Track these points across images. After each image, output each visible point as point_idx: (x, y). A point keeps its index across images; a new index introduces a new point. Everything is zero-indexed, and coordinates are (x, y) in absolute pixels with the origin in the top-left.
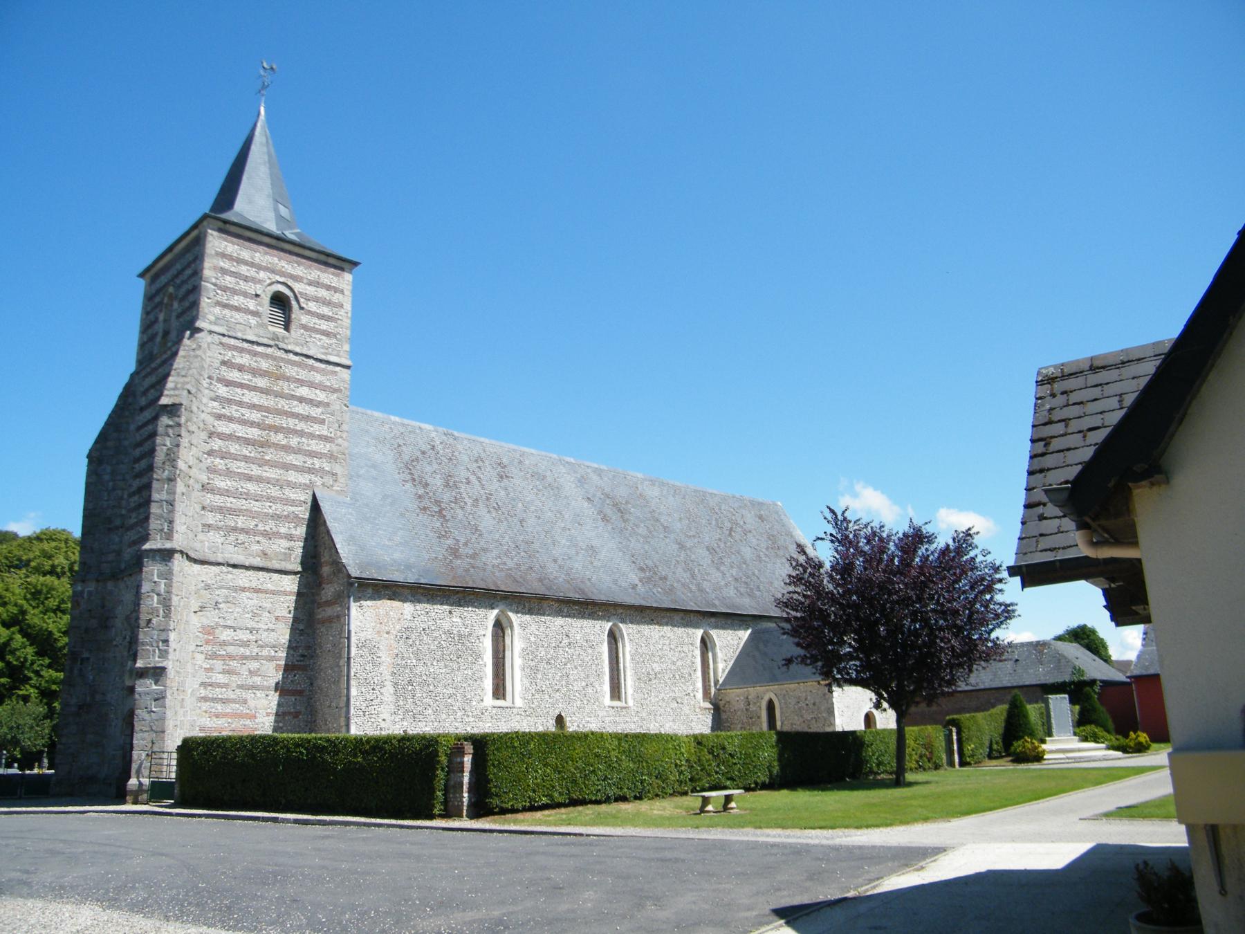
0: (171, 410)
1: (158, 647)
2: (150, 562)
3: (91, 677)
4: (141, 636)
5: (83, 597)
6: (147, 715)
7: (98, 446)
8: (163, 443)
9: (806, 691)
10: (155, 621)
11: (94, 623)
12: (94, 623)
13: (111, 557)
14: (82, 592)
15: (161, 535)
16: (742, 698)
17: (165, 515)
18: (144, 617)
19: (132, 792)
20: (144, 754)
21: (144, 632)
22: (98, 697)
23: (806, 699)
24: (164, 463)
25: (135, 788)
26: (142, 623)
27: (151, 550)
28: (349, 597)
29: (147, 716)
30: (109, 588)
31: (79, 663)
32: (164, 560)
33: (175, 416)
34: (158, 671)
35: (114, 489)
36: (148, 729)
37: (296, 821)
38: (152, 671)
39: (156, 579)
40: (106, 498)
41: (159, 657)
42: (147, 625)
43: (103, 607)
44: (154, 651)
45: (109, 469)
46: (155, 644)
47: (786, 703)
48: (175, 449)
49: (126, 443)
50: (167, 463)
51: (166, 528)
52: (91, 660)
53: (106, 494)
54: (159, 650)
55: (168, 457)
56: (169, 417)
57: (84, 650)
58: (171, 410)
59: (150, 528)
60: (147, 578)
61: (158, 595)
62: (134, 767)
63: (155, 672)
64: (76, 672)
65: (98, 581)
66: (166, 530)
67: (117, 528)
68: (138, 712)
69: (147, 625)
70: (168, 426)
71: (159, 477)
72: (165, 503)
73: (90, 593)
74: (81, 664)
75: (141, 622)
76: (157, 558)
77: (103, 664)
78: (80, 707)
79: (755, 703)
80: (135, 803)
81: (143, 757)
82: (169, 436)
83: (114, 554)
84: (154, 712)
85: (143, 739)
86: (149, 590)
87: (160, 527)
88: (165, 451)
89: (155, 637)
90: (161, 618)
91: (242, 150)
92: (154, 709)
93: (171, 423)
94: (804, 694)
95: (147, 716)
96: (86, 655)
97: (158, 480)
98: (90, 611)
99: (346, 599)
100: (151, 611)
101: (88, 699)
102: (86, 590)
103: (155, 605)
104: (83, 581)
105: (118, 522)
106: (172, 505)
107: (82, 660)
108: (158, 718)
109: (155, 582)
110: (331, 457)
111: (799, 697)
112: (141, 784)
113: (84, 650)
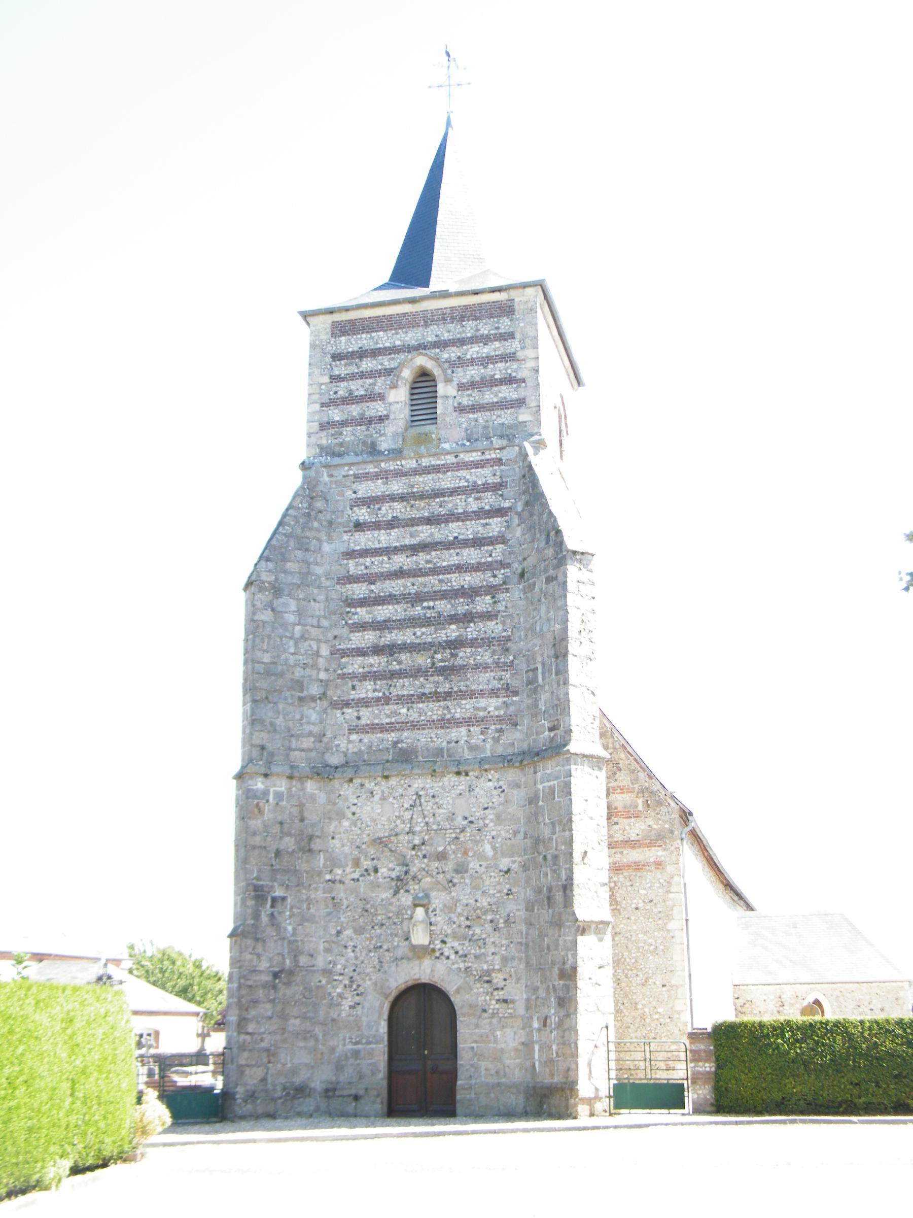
3: (290, 928)
11: (289, 843)
12: (289, 843)
13: (307, 743)
16: (772, 997)
22: (303, 960)
23: (655, 1029)
30: (309, 790)
31: (269, 903)
35: (303, 638)
37: (711, 1123)
40: (292, 650)
45: (293, 605)
47: (840, 1007)
52: (289, 900)
53: (291, 643)
57: (275, 884)
64: (264, 919)
73: (279, 796)
74: (272, 906)
77: (309, 909)
78: (276, 975)
79: (792, 1005)
83: (312, 739)
91: (441, 145)
94: (868, 997)
96: (279, 892)
98: (281, 823)
101: (288, 961)
107: (274, 900)
110: (351, 603)
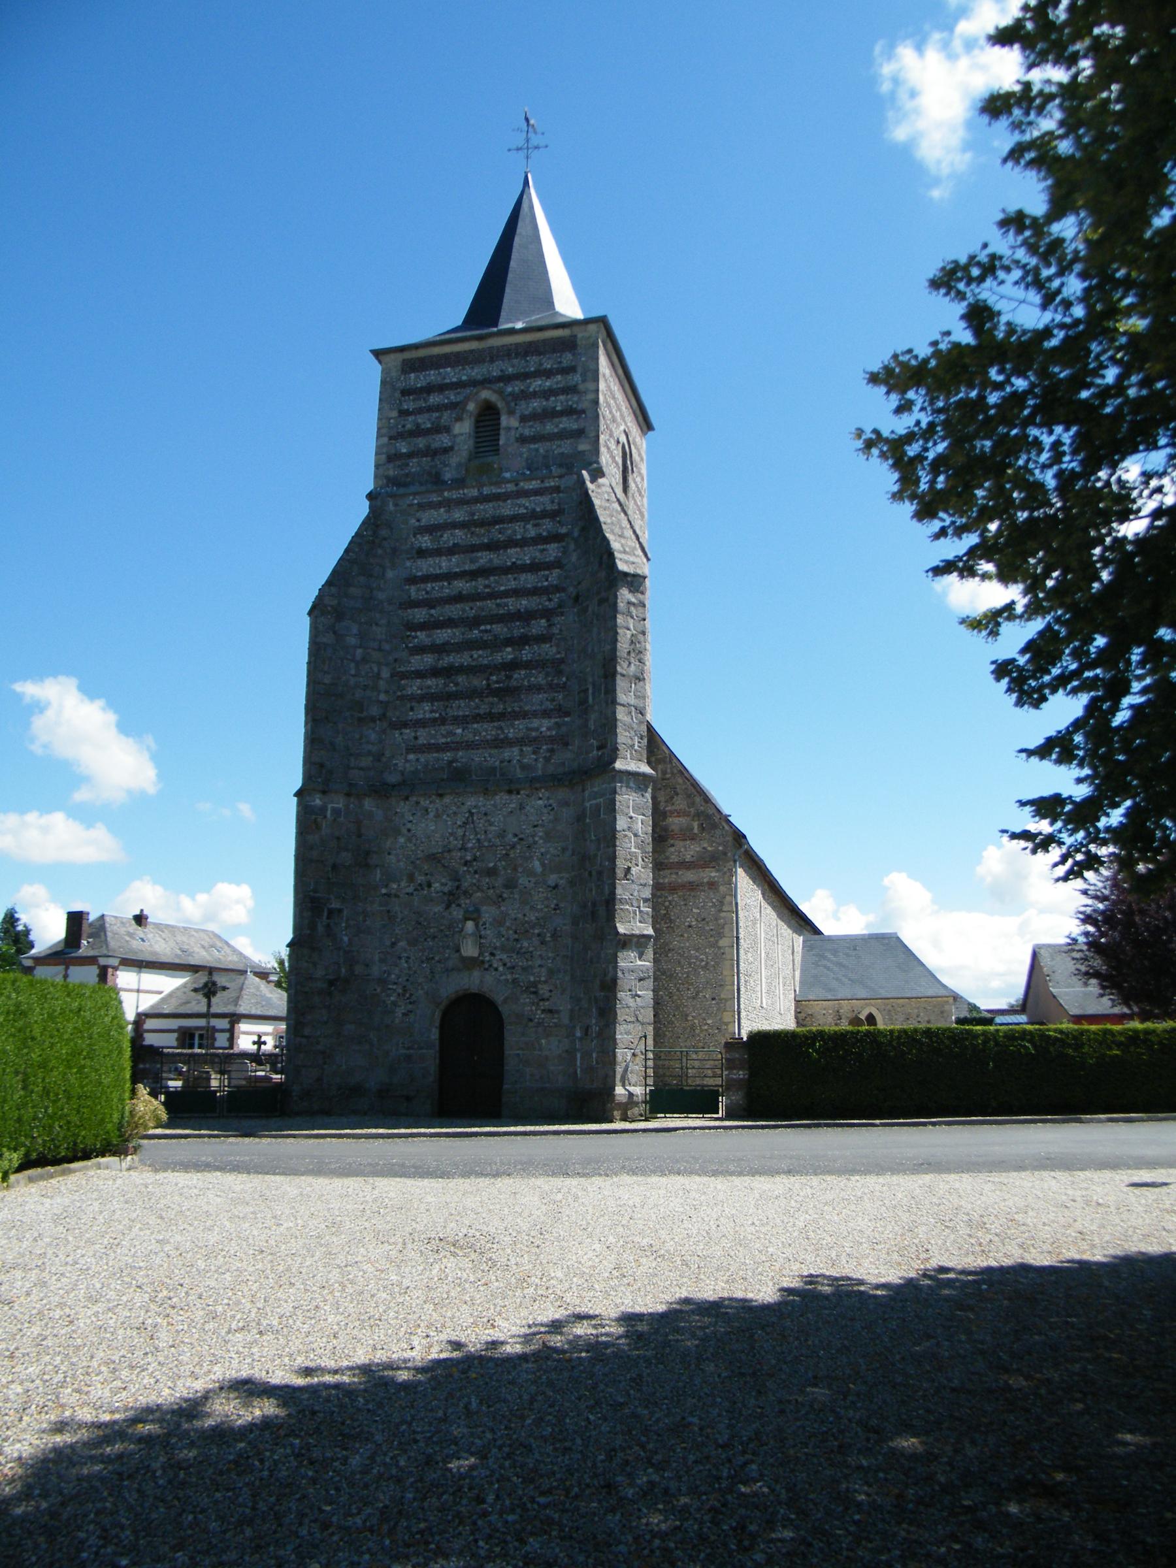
0: (632, 582)
1: (639, 907)
2: (624, 789)
3: (346, 939)
4: (619, 891)
5: (325, 817)
6: (632, 1000)
7: (333, 590)
8: (626, 627)
9: (918, 1008)
10: (634, 870)
11: (346, 857)
12: (346, 857)
13: (366, 762)
14: (323, 809)
15: (631, 754)
17: (635, 726)
18: (621, 864)
19: (620, 1104)
20: (629, 1053)
21: (622, 885)
24: (629, 653)
25: (624, 1100)
26: (620, 873)
27: (629, 774)
28: (735, 861)
29: (631, 1002)
32: (642, 790)
33: (637, 591)
34: (643, 940)
35: (365, 660)
36: (633, 1019)
38: (635, 939)
39: (632, 814)
41: (640, 922)
42: (626, 876)
43: (359, 836)
44: (635, 913)
46: (635, 904)
48: (641, 637)
49: (381, 596)
50: (633, 655)
51: (636, 743)
52: (345, 912)
53: (352, 665)
54: (641, 912)
55: (632, 647)
56: (630, 591)
58: (632, 582)
59: (619, 741)
60: (622, 811)
61: (636, 835)
62: (619, 1070)
63: (637, 943)
64: (321, 929)
65: (348, 795)
66: (636, 747)
67: (373, 719)
68: (620, 995)
69: (626, 876)
70: (629, 603)
71: (624, 672)
72: (633, 709)
73: (337, 812)
74: (328, 918)
75: (618, 871)
76: (632, 784)
78: (331, 983)
80: (625, 1119)
81: (629, 1058)
82: (632, 617)
84: (639, 996)
85: (628, 1033)
86: (625, 827)
87: (630, 742)
88: (629, 636)
89: (636, 894)
90: (639, 868)
92: (639, 993)
93: (633, 600)
95: (631, 1002)
96: (335, 905)
97: (623, 675)
98: (338, 838)
99: (732, 863)
100: (629, 857)
102: (330, 806)
103: (633, 850)
104: (324, 792)
105: (375, 711)
106: (641, 713)
107: (331, 912)
108: (644, 1004)
109: (631, 818)
111: (909, 1014)
112: (631, 1095)
113: (332, 896)
